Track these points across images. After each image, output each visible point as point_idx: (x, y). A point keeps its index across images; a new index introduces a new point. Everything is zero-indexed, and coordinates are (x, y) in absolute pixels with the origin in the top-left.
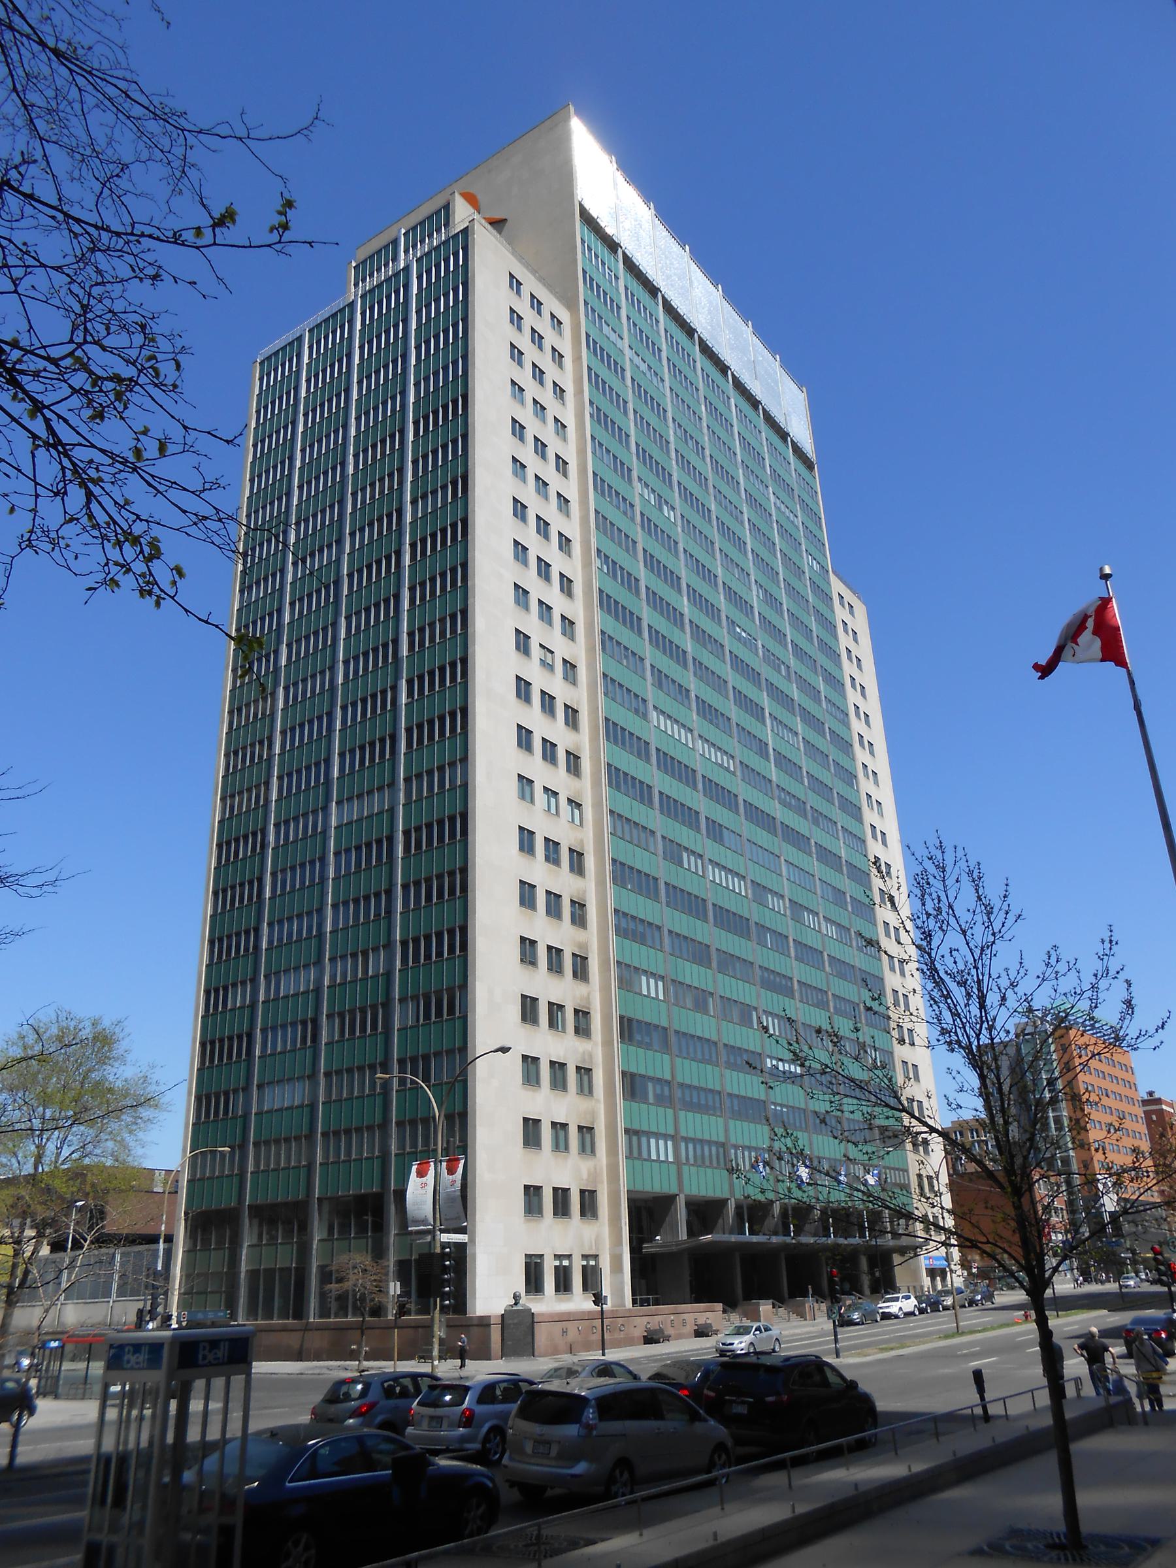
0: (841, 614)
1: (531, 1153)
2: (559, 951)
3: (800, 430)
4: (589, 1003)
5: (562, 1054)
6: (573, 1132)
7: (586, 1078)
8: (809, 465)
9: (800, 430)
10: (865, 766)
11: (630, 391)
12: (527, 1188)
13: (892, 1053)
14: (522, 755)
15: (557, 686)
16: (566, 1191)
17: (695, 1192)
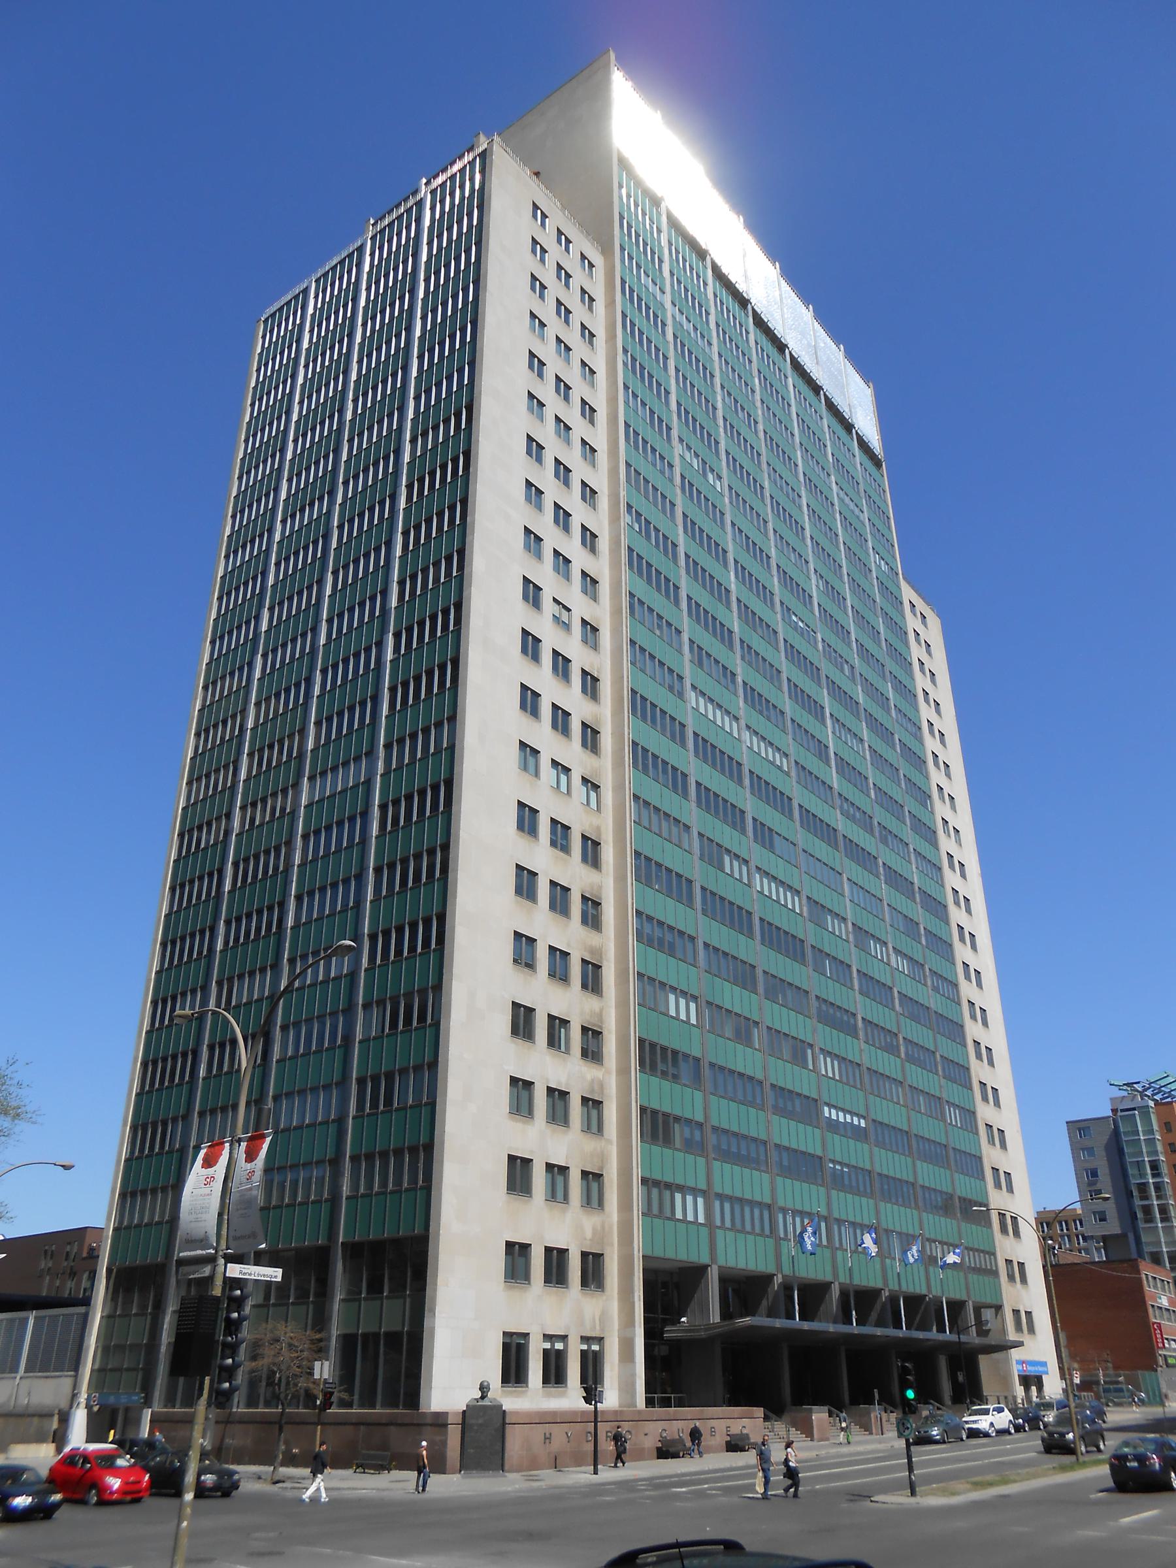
1: (517, 1202)
5: (563, 1080)
8: (877, 463)
12: (510, 1245)
14: (525, 719)
15: (572, 698)
16: (563, 1252)
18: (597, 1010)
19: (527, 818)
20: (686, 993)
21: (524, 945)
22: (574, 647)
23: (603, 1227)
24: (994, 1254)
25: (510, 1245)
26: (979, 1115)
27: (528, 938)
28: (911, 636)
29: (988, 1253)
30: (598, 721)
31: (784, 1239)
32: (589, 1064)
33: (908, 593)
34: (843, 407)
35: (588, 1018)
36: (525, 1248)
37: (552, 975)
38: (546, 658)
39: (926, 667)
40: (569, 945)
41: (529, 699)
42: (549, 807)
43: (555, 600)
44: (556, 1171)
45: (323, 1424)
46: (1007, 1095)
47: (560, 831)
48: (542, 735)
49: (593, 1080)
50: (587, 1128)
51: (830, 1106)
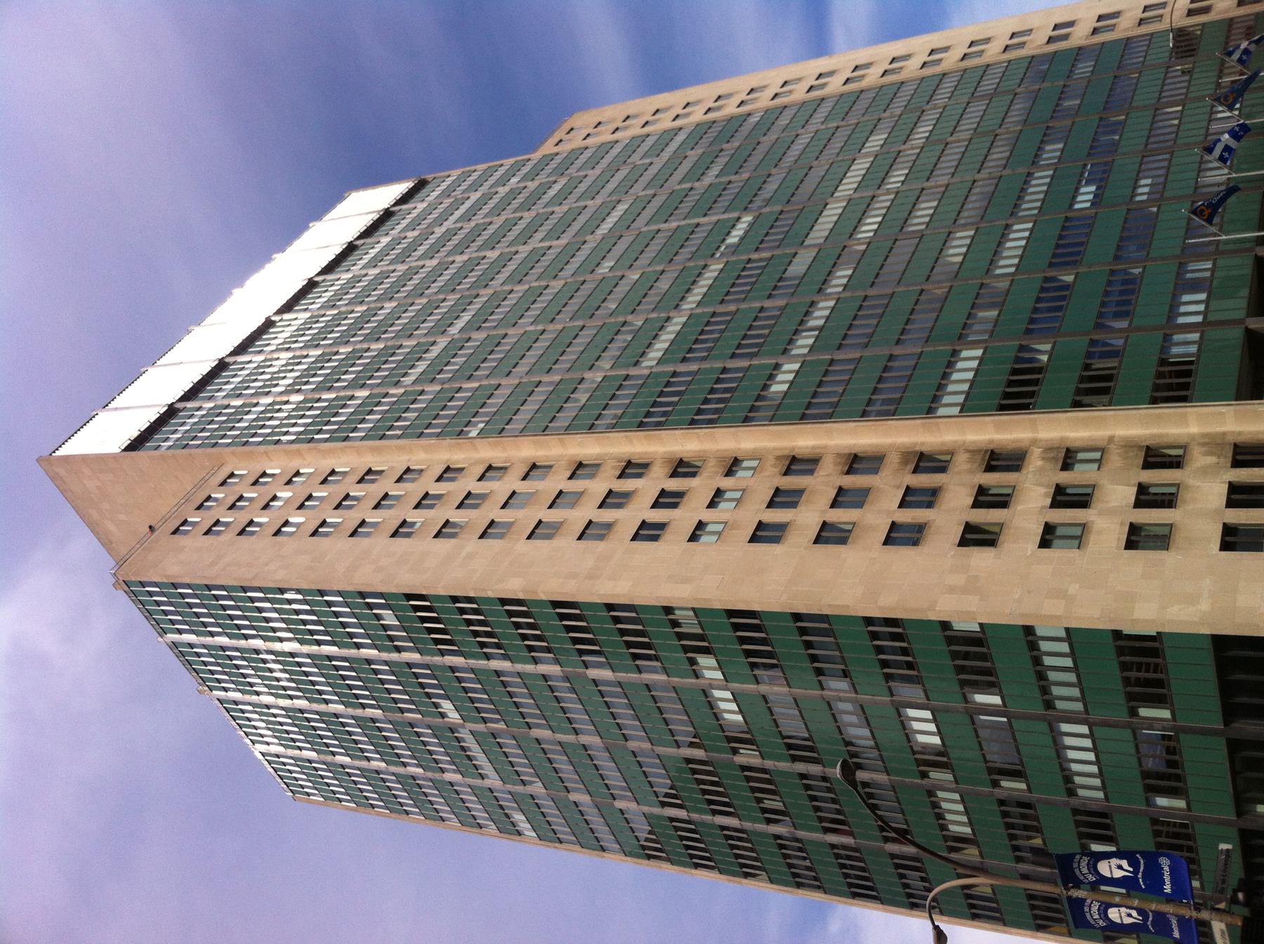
0: (576, 142)
1: (1178, 538)
2: (908, 490)
3: (385, 195)
4: (979, 451)
5: (1042, 490)
6: (991, 479)
7: (1081, 456)
8: (421, 185)
9: (385, 195)
10: (847, 81)
11: (755, 362)
12: (1225, 546)
13: (1080, 48)
14: (668, 536)
15: (647, 487)
16: (1233, 488)
17: (1243, 303)
18: (967, 455)
19: (763, 534)
20: (1163, 347)
21: (899, 535)
22: (647, 487)
23: (1204, 444)
24: (1231, 19)
25: (1225, 546)
26: (1130, 34)
27: (890, 531)
28: (711, 116)
29: (1230, 26)
30: (670, 460)
31: (1218, 246)
32: (1026, 463)
33: (548, 148)
34: (367, 221)
35: (976, 465)
36: (1134, 529)
37: (930, 505)
38: (608, 515)
39: (680, 111)
40: (898, 487)
41: (648, 532)
42: (756, 511)
43: (503, 507)
44: (1145, 498)
45: (1009, 722)
46: (897, 48)
47: (779, 499)
48: (681, 519)
49: (1043, 459)
50: (942, 468)
51: (1133, 195)
